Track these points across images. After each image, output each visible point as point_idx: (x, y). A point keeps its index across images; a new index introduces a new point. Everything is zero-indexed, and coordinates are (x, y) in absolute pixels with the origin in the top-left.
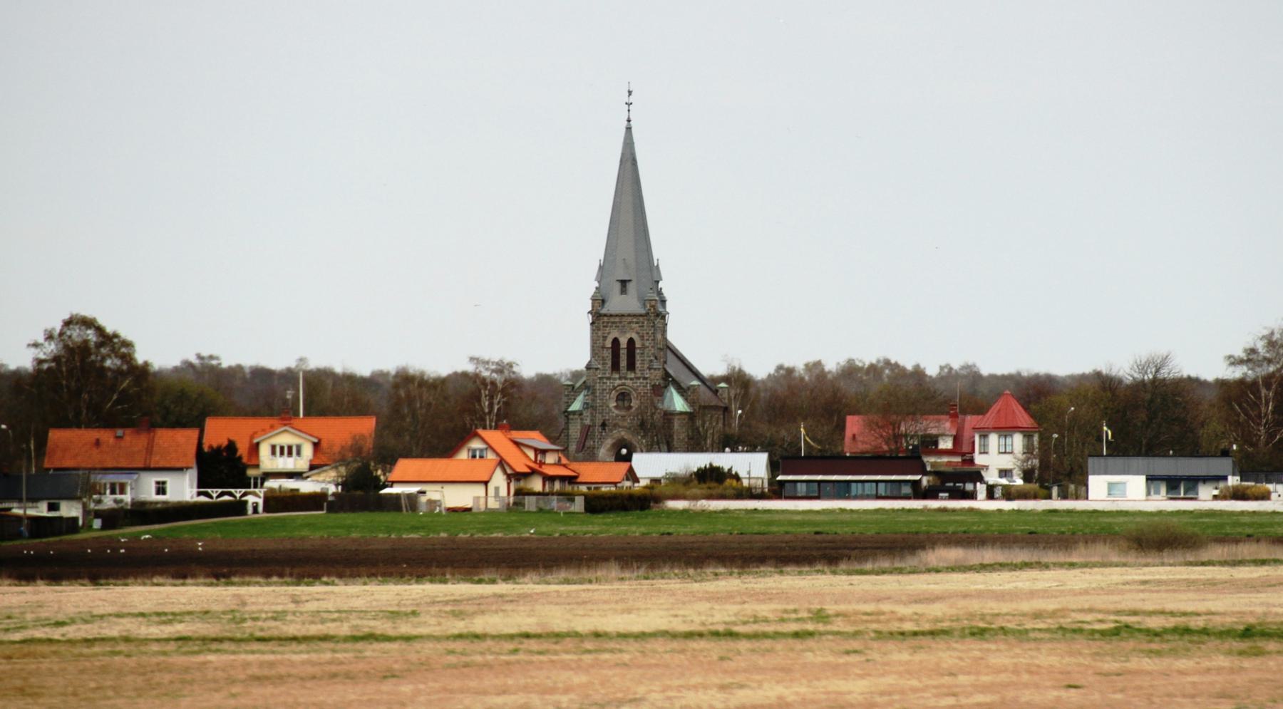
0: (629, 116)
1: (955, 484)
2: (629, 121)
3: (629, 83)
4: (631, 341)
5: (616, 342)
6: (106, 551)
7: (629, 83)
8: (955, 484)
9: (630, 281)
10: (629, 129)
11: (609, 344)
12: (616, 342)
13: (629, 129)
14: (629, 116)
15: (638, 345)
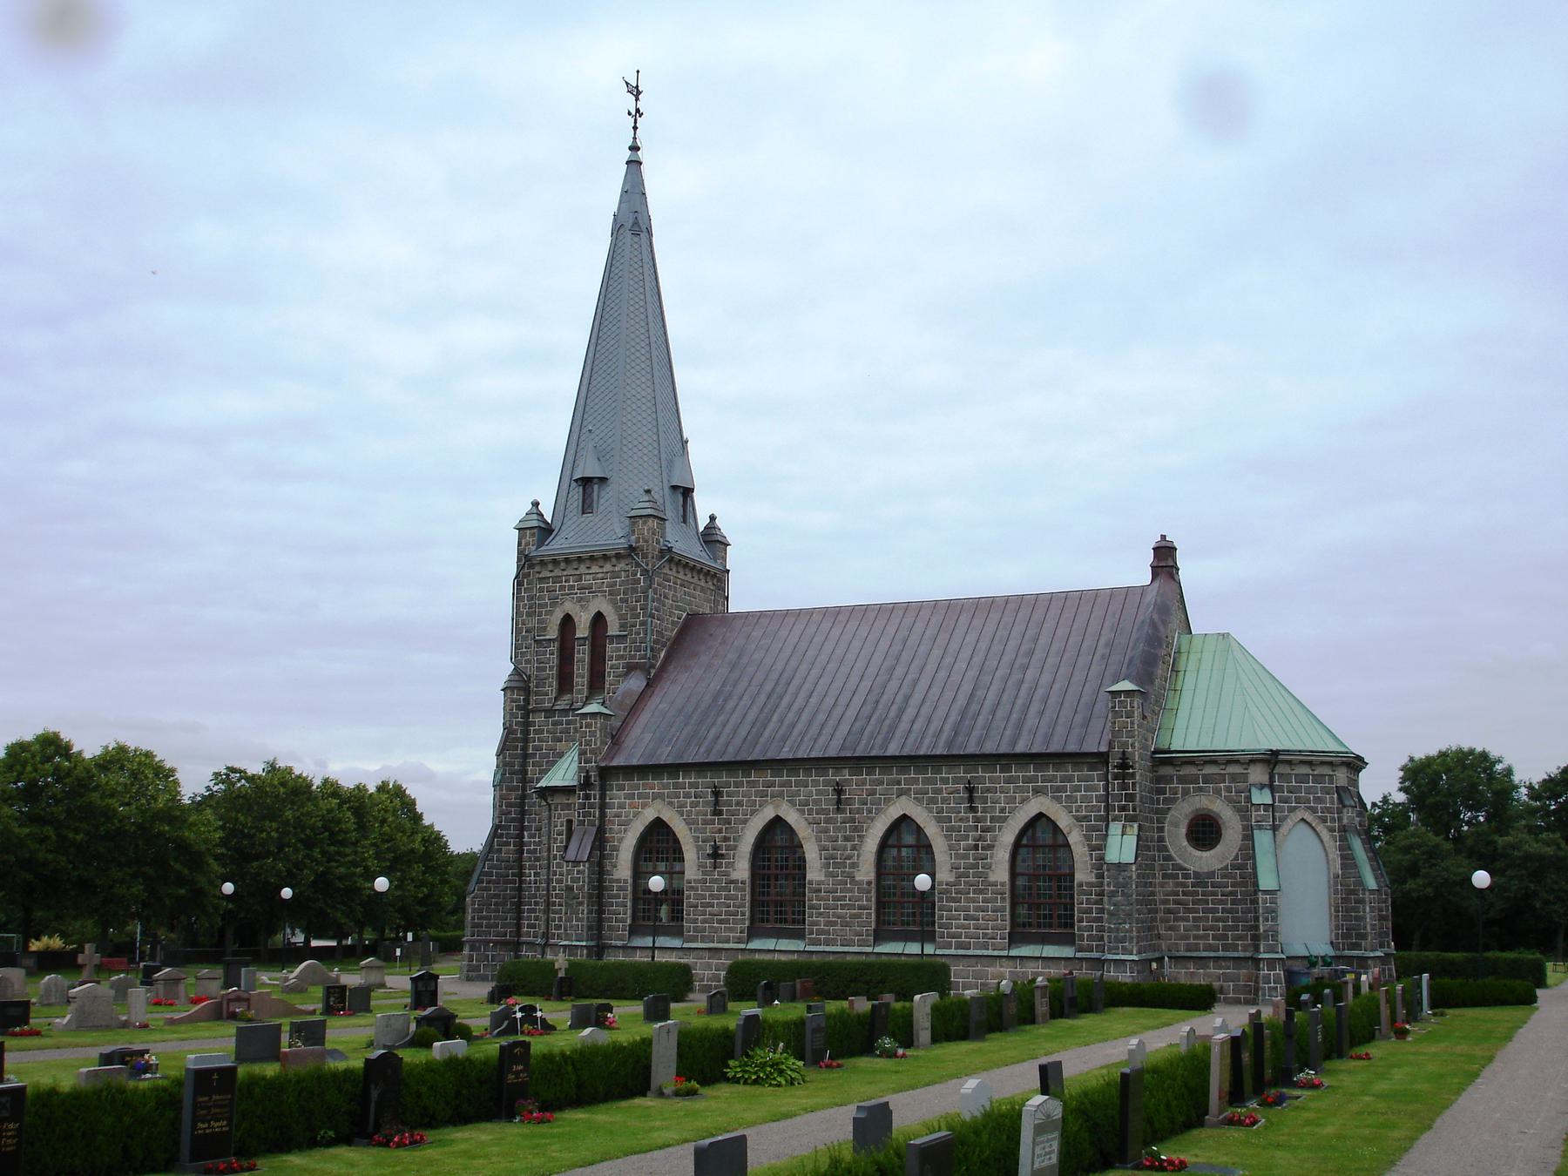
0: (635, 138)
1: (307, 941)
2: (634, 148)
3: (638, 72)
4: (599, 620)
5: (568, 622)
6: (1468, 880)
7: (638, 72)
8: (307, 941)
9: (603, 480)
10: (634, 164)
11: (553, 633)
12: (568, 622)
13: (634, 164)
14: (635, 138)
15: (613, 629)
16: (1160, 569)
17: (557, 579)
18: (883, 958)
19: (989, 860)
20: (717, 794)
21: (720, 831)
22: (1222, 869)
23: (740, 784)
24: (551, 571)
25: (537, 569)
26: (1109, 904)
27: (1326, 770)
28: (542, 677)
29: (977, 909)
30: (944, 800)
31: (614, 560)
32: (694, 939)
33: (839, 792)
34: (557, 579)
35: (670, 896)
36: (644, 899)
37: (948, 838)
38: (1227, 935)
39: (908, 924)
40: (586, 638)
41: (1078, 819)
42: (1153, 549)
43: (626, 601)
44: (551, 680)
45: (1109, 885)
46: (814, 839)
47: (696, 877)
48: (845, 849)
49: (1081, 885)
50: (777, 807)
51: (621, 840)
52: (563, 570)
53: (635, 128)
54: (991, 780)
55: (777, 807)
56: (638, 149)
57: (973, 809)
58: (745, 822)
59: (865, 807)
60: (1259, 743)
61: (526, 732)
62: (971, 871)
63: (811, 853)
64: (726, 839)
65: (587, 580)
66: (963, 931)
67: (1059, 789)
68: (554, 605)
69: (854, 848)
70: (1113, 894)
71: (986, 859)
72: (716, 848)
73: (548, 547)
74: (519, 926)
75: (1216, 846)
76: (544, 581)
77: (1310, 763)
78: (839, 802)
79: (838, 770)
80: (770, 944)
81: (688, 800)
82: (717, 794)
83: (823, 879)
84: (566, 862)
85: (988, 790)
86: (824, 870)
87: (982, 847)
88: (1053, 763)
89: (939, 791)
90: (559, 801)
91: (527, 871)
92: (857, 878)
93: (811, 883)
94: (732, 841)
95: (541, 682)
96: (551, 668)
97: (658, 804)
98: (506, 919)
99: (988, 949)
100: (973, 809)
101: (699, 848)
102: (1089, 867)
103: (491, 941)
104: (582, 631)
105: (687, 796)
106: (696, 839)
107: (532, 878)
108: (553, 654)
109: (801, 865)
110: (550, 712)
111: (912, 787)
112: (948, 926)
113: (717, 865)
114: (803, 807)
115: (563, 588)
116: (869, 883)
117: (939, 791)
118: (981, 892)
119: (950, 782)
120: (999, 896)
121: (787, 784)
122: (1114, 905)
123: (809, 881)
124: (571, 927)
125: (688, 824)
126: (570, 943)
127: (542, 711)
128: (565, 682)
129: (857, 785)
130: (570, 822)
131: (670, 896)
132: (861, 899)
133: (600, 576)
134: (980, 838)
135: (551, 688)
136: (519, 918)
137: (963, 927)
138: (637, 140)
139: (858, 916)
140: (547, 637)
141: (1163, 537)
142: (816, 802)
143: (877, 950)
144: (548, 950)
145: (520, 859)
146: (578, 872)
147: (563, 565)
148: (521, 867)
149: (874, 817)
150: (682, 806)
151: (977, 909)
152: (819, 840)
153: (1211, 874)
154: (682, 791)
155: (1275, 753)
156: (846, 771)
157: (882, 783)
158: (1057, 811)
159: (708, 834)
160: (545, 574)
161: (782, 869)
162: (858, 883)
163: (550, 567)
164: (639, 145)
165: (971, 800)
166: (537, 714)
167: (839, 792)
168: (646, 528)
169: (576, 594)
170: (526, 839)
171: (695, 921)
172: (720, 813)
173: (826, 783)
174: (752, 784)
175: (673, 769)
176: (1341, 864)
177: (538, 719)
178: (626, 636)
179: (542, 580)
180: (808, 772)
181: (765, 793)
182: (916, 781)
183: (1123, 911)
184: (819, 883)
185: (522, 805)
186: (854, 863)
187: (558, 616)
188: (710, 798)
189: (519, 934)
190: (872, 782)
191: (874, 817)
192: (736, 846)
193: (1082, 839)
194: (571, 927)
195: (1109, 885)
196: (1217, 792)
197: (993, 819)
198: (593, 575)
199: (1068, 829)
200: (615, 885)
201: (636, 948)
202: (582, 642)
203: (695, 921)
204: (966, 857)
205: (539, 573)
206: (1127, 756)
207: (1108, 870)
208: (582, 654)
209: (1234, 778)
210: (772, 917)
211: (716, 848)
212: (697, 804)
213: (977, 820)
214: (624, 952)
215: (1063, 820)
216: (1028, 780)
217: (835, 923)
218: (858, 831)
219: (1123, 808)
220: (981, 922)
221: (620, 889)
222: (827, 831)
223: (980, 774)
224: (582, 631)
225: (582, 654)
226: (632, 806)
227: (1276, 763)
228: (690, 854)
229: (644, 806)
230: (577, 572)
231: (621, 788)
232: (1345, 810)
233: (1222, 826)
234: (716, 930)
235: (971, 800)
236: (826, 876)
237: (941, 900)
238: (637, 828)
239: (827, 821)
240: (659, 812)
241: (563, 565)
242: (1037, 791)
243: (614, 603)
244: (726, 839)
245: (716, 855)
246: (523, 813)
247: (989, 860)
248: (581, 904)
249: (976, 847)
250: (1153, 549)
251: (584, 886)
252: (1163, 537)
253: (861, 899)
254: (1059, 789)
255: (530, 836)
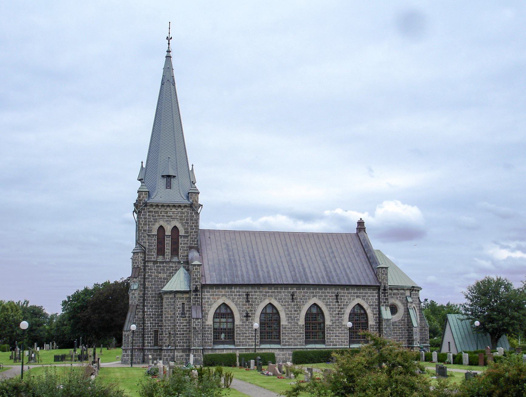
0: (169, 48)
2: (169, 51)
3: (170, 23)
7: (170, 23)
9: (174, 177)
10: (168, 57)
11: (155, 232)
13: (168, 57)
14: (169, 48)
15: (182, 232)
16: (361, 229)
17: (155, 212)
18: (308, 350)
19: (343, 318)
20: (247, 295)
21: (249, 308)
22: (398, 321)
23: (256, 292)
24: (154, 209)
25: (148, 207)
26: (385, 331)
27: (402, 291)
28: (151, 249)
29: (339, 333)
30: (328, 299)
31: (183, 208)
32: (239, 345)
33: (293, 295)
34: (155, 212)
35: (227, 330)
36: (217, 332)
37: (330, 311)
38: (400, 340)
39: (314, 339)
40: (169, 235)
41: (370, 305)
42: (357, 223)
43: (188, 223)
44: (154, 250)
45: (384, 326)
46: (283, 311)
47: (239, 324)
48: (295, 314)
49: (371, 325)
50: (270, 300)
51: (209, 311)
52: (154, 209)
53: (169, 44)
54: (343, 293)
55: (270, 300)
56: (170, 52)
57: (337, 302)
58: (258, 305)
59: (302, 300)
60: (402, 284)
61: (145, 269)
62: (337, 321)
63: (283, 315)
64: (251, 311)
65: (170, 214)
66: (335, 340)
67: (365, 296)
68: (155, 222)
69: (298, 314)
70: (386, 328)
71: (342, 317)
72: (247, 314)
73: (153, 200)
74: (143, 343)
75: (396, 314)
76: (151, 212)
77: (397, 289)
78: (293, 299)
79: (292, 288)
80: (268, 346)
81: (236, 297)
82: (247, 295)
83: (287, 324)
84: (193, 318)
85: (342, 296)
86: (287, 321)
87: (340, 314)
88: (362, 288)
89: (326, 296)
90: (179, 296)
91: (147, 322)
92: (299, 324)
93: (283, 325)
94: (253, 311)
95: (150, 251)
96: (155, 246)
97: (224, 298)
98: (395, 336)
99: (342, 346)
100: (337, 302)
101: (240, 314)
102: (373, 320)
103: (136, 349)
104: (168, 232)
105: (235, 295)
106: (240, 311)
107: (149, 325)
108: (155, 240)
109: (278, 320)
110: (155, 262)
111: (318, 294)
112: (330, 339)
113: (248, 320)
114: (279, 301)
115: (159, 216)
116: (303, 325)
117: (326, 296)
118: (340, 328)
119: (330, 293)
120: (346, 329)
121: (274, 292)
122: (386, 331)
123: (282, 325)
124: (196, 342)
125: (236, 305)
126: (196, 348)
127: (151, 262)
128: (161, 251)
129: (299, 293)
130: (183, 304)
131: (227, 330)
132: (301, 331)
133: (176, 213)
134: (340, 311)
135: (154, 253)
136: (143, 340)
137: (335, 339)
138: (170, 48)
139: (300, 336)
140: (152, 234)
141: (361, 219)
142: (284, 299)
143: (306, 347)
144: (175, 351)
145: (144, 318)
146: (198, 322)
147: (160, 207)
148: (144, 320)
149: (305, 304)
150: (233, 299)
151: (339, 333)
152: (285, 311)
153: (396, 322)
154: (234, 294)
155: (413, 287)
156: (367, 289)
157: (307, 293)
158: (363, 303)
159: (244, 309)
160: (151, 209)
161: (269, 321)
162: (299, 325)
163: (154, 207)
164: (171, 50)
165: (337, 299)
166: (149, 263)
167: (293, 295)
168: (196, 197)
169: (165, 218)
170: (146, 310)
171: (240, 339)
172: (249, 301)
173: (289, 292)
174: (261, 292)
175: (230, 286)
176: (420, 319)
177: (150, 264)
178: (189, 236)
179: (149, 212)
180: (281, 288)
181: (266, 295)
182: (319, 293)
183: (389, 333)
184: (286, 325)
185: (144, 297)
186: (253, 319)
187: (157, 226)
188: (245, 296)
189: (143, 346)
190: (304, 293)
191: (305, 304)
192: (255, 313)
193: (371, 311)
194: (196, 342)
195: (384, 326)
196: (397, 298)
197: (344, 305)
198: (172, 212)
199: (367, 308)
200: (206, 327)
201: (216, 349)
202: (169, 237)
203: (240, 339)
204: (336, 317)
205: (149, 209)
206: (386, 286)
207: (384, 321)
208: (168, 242)
209: (402, 294)
210: (311, 337)
211: (247, 314)
212: (240, 298)
213: (339, 305)
214: (177, 351)
215: (365, 306)
216: (354, 293)
217: (291, 339)
218: (299, 309)
219: (385, 302)
220: (340, 337)
221: (209, 328)
222: (288, 308)
223: (340, 291)
224: (168, 232)
225: (168, 242)
226: (213, 298)
227: (413, 290)
228: (237, 316)
229: (218, 299)
230: (166, 210)
231: (208, 292)
232: (408, 303)
233: (398, 308)
234: (248, 342)
235: (337, 299)
236: (288, 323)
237: (327, 331)
238: (215, 306)
239: (289, 305)
240: (224, 301)
241: (154, 207)
242: (357, 297)
243: (182, 224)
244: (251, 311)
245: (247, 316)
246: (144, 300)
247: (343, 318)
248: (200, 334)
249: (339, 314)
250: (357, 223)
251: (200, 327)
252: (361, 219)
253: (301, 331)
254: (365, 296)
255: (148, 309)
